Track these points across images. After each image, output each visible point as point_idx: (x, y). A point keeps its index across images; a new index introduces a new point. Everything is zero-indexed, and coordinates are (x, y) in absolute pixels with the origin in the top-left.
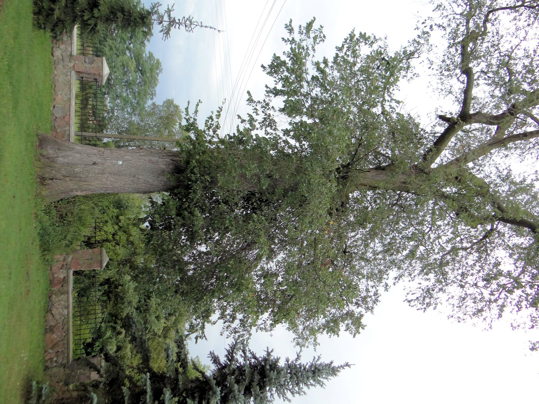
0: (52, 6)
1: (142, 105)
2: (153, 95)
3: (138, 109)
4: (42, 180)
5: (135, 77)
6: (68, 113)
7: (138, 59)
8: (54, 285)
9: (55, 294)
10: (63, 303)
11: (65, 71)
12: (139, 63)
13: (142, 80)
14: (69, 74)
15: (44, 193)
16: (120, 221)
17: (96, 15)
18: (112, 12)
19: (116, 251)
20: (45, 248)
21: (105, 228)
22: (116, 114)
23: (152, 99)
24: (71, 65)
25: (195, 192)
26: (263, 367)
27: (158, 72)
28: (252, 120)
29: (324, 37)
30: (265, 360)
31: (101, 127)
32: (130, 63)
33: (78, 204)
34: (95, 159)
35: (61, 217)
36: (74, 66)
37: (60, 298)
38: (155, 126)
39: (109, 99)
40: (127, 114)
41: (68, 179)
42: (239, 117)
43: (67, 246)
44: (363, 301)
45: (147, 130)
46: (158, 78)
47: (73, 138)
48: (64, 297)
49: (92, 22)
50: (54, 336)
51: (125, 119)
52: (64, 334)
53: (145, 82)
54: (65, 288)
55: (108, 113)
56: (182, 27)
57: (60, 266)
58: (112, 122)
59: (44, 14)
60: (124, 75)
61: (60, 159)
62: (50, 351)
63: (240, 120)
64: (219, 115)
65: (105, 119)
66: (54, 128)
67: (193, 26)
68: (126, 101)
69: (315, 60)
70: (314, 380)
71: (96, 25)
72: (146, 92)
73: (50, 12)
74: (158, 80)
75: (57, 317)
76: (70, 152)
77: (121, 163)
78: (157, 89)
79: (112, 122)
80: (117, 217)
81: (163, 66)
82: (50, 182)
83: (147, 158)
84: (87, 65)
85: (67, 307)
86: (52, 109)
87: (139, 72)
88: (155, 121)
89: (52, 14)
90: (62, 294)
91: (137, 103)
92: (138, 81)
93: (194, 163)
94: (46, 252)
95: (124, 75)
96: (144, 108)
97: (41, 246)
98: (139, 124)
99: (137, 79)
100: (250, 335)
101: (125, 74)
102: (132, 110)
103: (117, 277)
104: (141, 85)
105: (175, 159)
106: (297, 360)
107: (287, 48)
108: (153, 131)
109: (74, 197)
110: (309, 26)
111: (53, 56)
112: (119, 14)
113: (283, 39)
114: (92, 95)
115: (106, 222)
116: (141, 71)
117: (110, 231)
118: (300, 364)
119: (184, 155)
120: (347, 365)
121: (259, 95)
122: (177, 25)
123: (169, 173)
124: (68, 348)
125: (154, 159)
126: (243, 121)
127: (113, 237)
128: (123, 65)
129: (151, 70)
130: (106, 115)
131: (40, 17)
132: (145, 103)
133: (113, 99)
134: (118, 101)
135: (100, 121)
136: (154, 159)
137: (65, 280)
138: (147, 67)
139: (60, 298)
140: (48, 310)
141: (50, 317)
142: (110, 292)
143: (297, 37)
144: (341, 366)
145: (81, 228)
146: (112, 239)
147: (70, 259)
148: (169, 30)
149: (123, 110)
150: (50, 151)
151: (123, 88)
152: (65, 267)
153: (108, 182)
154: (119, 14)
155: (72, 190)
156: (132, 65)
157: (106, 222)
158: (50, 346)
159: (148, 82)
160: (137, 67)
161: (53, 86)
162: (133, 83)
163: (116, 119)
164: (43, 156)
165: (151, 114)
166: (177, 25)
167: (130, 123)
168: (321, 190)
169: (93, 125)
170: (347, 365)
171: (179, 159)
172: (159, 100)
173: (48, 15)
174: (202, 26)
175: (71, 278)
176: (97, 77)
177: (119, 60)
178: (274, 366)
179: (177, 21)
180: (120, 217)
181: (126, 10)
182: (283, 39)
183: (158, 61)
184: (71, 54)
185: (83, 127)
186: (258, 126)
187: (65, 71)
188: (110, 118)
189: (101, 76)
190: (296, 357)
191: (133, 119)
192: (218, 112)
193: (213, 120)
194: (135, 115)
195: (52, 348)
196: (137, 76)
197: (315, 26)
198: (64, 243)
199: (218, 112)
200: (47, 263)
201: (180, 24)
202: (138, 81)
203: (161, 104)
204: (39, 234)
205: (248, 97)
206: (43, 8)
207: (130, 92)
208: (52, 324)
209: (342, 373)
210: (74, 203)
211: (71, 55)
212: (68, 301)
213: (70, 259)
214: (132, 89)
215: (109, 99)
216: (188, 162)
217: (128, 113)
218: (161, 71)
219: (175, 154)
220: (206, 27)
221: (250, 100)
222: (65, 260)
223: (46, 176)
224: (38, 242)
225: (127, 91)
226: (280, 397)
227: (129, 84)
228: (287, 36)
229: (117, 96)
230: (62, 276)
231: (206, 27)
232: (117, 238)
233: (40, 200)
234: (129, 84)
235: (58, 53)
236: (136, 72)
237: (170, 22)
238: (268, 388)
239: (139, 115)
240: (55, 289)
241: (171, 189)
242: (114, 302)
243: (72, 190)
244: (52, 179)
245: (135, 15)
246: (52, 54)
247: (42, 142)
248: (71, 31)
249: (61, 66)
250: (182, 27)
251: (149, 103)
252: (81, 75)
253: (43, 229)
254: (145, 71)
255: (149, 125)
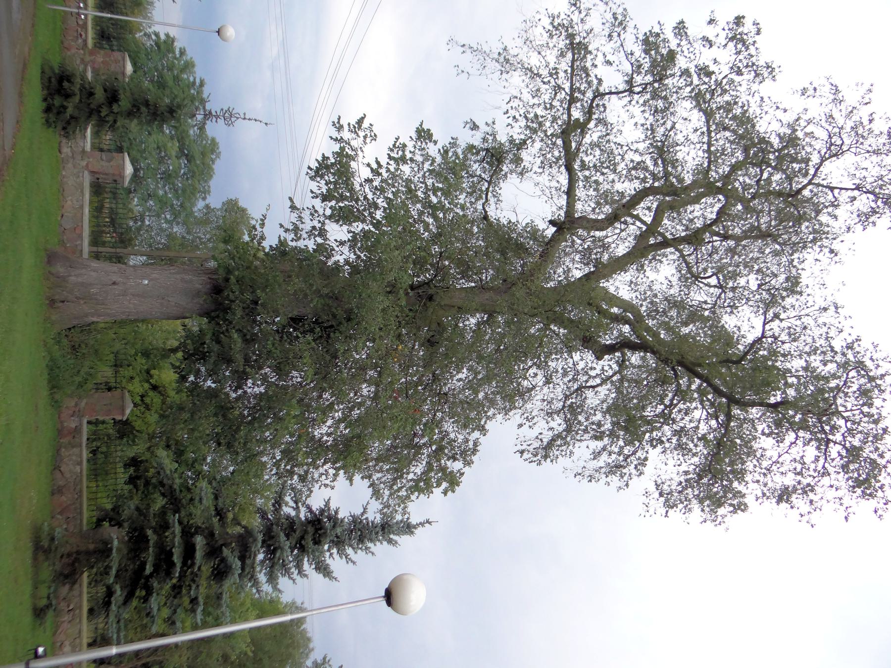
0: (65, 103)
1: (189, 209)
2: (206, 192)
3: (183, 215)
4: (52, 302)
5: (177, 165)
6: (80, 224)
7: (182, 138)
8: (63, 436)
9: (65, 448)
10: (74, 458)
11: (75, 171)
12: (184, 144)
13: (189, 170)
14: (81, 175)
15: (53, 318)
16: (151, 376)
17: (116, 111)
18: (134, 106)
19: (146, 420)
20: (54, 385)
21: (130, 387)
22: (147, 223)
23: (204, 199)
24: (84, 163)
25: (234, 314)
26: (319, 521)
27: (213, 157)
28: (296, 230)
29: (375, 135)
30: (322, 511)
31: (124, 240)
32: (170, 145)
33: (94, 333)
34: (115, 278)
35: (75, 350)
36: (87, 164)
37: (71, 452)
38: (209, 240)
39: (136, 200)
40: (165, 223)
41: (82, 302)
42: (281, 226)
43: (80, 385)
44: (461, 455)
45: (197, 246)
46: (214, 167)
47: (86, 254)
48: (76, 450)
49: (110, 119)
50: (64, 498)
51: (162, 230)
52: (76, 496)
53: (194, 172)
54: (77, 440)
55: (135, 222)
56: (221, 121)
57: (71, 412)
58: (141, 236)
59: (55, 111)
60: (160, 163)
61: (73, 278)
62: (59, 516)
63: (282, 229)
64: (263, 224)
65: (131, 230)
66: (62, 243)
67: (233, 119)
68: (163, 203)
69: (366, 161)
70: (383, 537)
71: (115, 121)
72: (195, 189)
73: (62, 109)
74: (213, 170)
75: (68, 475)
76: (84, 270)
77: (146, 282)
78: (212, 183)
79: (141, 236)
80: (148, 372)
81: (222, 148)
82: (61, 304)
83: (178, 276)
84: (104, 164)
85: (80, 463)
86: (59, 218)
87: (184, 158)
88: (208, 232)
89: (65, 112)
90: (73, 447)
91: (182, 206)
92: (182, 171)
93: (233, 279)
94: (55, 390)
95: (160, 163)
96: (192, 212)
97: (49, 382)
98: (183, 237)
99: (180, 168)
100: (311, 492)
101: (161, 160)
102: (173, 217)
103: (148, 455)
104: (187, 179)
105: (214, 277)
106: (362, 514)
107: (336, 148)
108: (206, 248)
109: (89, 325)
110: (360, 122)
111: (60, 151)
112: (143, 109)
113: (331, 138)
114: (109, 195)
115: (132, 378)
116: (187, 156)
117: (137, 390)
118: (367, 519)
119: (221, 271)
120: (428, 522)
121: (306, 201)
122: (214, 119)
123: (206, 294)
124: (81, 513)
125: (188, 277)
126: (287, 230)
127: (142, 400)
128: (158, 147)
129: (203, 154)
130: (131, 224)
131: (51, 115)
132: (193, 205)
133: (144, 200)
134: (151, 202)
135: (122, 234)
136: (188, 277)
137: (77, 430)
138: (196, 151)
139: (71, 452)
140: (56, 468)
141: (59, 475)
142: (138, 478)
143: (346, 135)
144: (420, 523)
145: (98, 363)
146: (140, 402)
147: (83, 404)
148: (205, 124)
149: (158, 216)
150: (60, 269)
151: (158, 183)
152: (77, 413)
153: (131, 306)
154: (143, 109)
155: (86, 315)
156: (173, 147)
157: (132, 378)
158: (59, 511)
159: (197, 174)
160: (181, 149)
161: (61, 190)
162: (174, 175)
163: (147, 231)
164: (53, 274)
165: (204, 221)
166: (214, 119)
167: (171, 237)
168: (419, 315)
169: (113, 236)
170: (428, 522)
171: (216, 277)
172: (215, 200)
173: (59, 113)
174: (245, 119)
175: (85, 428)
176: (116, 178)
177: (151, 139)
178: (334, 520)
179: (214, 113)
180: (152, 372)
181: (151, 103)
182: (331, 138)
183: (213, 140)
184: (84, 149)
185: (96, 241)
186: (305, 236)
187: (75, 171)
188: (139, 229)
189: (122, 177)
190: (362, 510)
191: (175, 230)
192: (262, 220)
193: (256, 230)
194: (178, 224)
195: (61, 513)
196: (180, 164)
197: (365, 124)
198: (78, 379)
199: (262, 220)
200: (56, 404)
201: (217, 117)
202: (182, 171)
203: (219, 206)
204: (47, 366)
205: (289, 204)
206: (54, 105)
207: (170, 189)
208: (61, 483)
209: (419, 531)
210: (90, 331)
211: (83, 151)
212: (81, 456)
213: (83, 404)
214: (173, 184)
215: (136, 200)
216: (227, 280)
217: (167, 221)
218: (218, 156)
219: (215, 271)
220: (249, 119)
221: (293, 208)
222: (76, 405)
223: (57, 297)
224: (46, 376)
225: (164, 186)
226: (341, 558)
227: (168, 177)
228: (335, 135)
229: (149, 195)
230: (73, 425)
231: (249, 119)
232: (148, 400)
233: (49, 325)
234: (168, 177)
235: (66, 150)
236: (178, 158)
237: (205, 115)
238: (326, 547)
239: (184, 223)
240: (64, 441)
241: (206, 314)
242: (143, 492)
243: (86, 315)
244: (63, 302)
245: (162, 109)
246: (60, 151)
247: (51, 258)
248: (86, 129)
249: (70, 165)
250: (221, 121)
251: (201, 204)
252: (97, 176)
253: (52, 360)
254: (193, 157)
255: (200, 238)
